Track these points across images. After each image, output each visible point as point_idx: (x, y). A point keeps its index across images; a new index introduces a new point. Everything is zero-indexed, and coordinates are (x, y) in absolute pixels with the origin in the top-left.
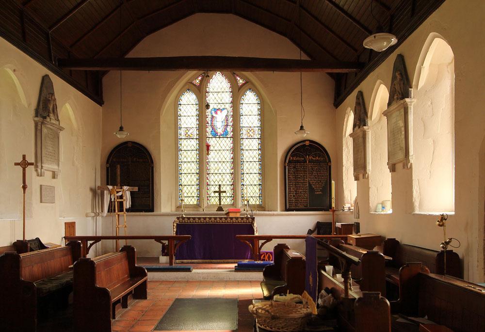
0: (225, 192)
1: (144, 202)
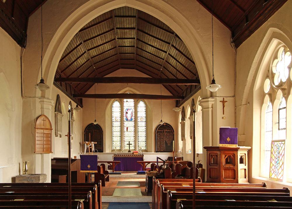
0: (131, 144)
1: (100, 148)
